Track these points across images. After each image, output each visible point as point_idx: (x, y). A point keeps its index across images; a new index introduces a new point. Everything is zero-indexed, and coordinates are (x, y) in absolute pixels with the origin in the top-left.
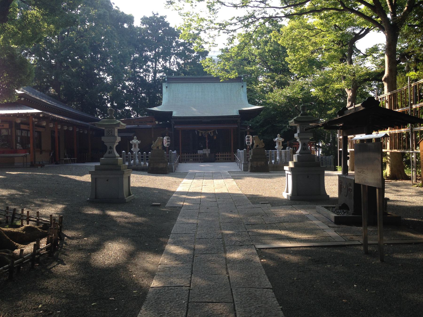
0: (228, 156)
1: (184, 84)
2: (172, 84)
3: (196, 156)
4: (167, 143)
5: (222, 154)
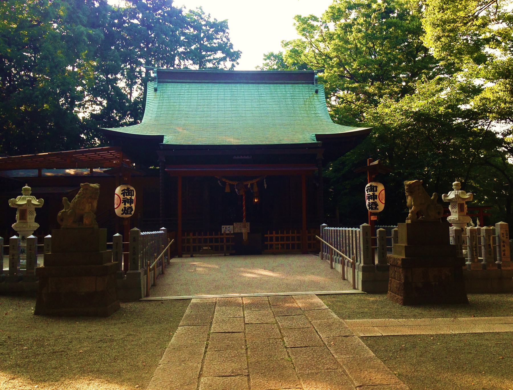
0: (288, 239)
1: (194, 85)
2: (168, 84)
3: (217, 241)
4: (122, 206)
5: (279, 235)
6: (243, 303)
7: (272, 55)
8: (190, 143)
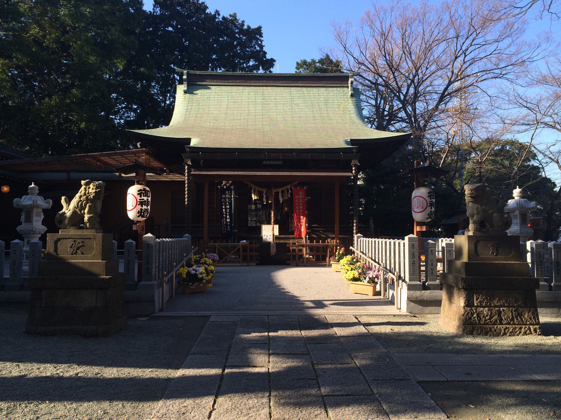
6: (269, 323)
7: (305, 62)
8: (218, 146)
